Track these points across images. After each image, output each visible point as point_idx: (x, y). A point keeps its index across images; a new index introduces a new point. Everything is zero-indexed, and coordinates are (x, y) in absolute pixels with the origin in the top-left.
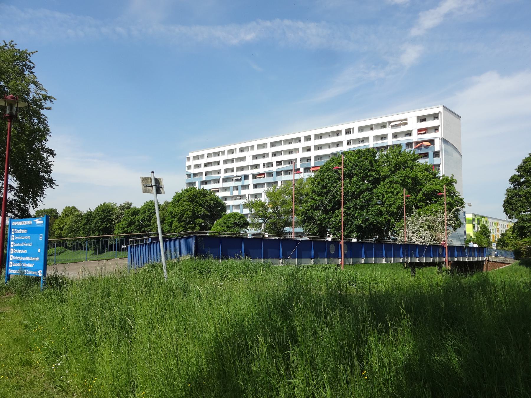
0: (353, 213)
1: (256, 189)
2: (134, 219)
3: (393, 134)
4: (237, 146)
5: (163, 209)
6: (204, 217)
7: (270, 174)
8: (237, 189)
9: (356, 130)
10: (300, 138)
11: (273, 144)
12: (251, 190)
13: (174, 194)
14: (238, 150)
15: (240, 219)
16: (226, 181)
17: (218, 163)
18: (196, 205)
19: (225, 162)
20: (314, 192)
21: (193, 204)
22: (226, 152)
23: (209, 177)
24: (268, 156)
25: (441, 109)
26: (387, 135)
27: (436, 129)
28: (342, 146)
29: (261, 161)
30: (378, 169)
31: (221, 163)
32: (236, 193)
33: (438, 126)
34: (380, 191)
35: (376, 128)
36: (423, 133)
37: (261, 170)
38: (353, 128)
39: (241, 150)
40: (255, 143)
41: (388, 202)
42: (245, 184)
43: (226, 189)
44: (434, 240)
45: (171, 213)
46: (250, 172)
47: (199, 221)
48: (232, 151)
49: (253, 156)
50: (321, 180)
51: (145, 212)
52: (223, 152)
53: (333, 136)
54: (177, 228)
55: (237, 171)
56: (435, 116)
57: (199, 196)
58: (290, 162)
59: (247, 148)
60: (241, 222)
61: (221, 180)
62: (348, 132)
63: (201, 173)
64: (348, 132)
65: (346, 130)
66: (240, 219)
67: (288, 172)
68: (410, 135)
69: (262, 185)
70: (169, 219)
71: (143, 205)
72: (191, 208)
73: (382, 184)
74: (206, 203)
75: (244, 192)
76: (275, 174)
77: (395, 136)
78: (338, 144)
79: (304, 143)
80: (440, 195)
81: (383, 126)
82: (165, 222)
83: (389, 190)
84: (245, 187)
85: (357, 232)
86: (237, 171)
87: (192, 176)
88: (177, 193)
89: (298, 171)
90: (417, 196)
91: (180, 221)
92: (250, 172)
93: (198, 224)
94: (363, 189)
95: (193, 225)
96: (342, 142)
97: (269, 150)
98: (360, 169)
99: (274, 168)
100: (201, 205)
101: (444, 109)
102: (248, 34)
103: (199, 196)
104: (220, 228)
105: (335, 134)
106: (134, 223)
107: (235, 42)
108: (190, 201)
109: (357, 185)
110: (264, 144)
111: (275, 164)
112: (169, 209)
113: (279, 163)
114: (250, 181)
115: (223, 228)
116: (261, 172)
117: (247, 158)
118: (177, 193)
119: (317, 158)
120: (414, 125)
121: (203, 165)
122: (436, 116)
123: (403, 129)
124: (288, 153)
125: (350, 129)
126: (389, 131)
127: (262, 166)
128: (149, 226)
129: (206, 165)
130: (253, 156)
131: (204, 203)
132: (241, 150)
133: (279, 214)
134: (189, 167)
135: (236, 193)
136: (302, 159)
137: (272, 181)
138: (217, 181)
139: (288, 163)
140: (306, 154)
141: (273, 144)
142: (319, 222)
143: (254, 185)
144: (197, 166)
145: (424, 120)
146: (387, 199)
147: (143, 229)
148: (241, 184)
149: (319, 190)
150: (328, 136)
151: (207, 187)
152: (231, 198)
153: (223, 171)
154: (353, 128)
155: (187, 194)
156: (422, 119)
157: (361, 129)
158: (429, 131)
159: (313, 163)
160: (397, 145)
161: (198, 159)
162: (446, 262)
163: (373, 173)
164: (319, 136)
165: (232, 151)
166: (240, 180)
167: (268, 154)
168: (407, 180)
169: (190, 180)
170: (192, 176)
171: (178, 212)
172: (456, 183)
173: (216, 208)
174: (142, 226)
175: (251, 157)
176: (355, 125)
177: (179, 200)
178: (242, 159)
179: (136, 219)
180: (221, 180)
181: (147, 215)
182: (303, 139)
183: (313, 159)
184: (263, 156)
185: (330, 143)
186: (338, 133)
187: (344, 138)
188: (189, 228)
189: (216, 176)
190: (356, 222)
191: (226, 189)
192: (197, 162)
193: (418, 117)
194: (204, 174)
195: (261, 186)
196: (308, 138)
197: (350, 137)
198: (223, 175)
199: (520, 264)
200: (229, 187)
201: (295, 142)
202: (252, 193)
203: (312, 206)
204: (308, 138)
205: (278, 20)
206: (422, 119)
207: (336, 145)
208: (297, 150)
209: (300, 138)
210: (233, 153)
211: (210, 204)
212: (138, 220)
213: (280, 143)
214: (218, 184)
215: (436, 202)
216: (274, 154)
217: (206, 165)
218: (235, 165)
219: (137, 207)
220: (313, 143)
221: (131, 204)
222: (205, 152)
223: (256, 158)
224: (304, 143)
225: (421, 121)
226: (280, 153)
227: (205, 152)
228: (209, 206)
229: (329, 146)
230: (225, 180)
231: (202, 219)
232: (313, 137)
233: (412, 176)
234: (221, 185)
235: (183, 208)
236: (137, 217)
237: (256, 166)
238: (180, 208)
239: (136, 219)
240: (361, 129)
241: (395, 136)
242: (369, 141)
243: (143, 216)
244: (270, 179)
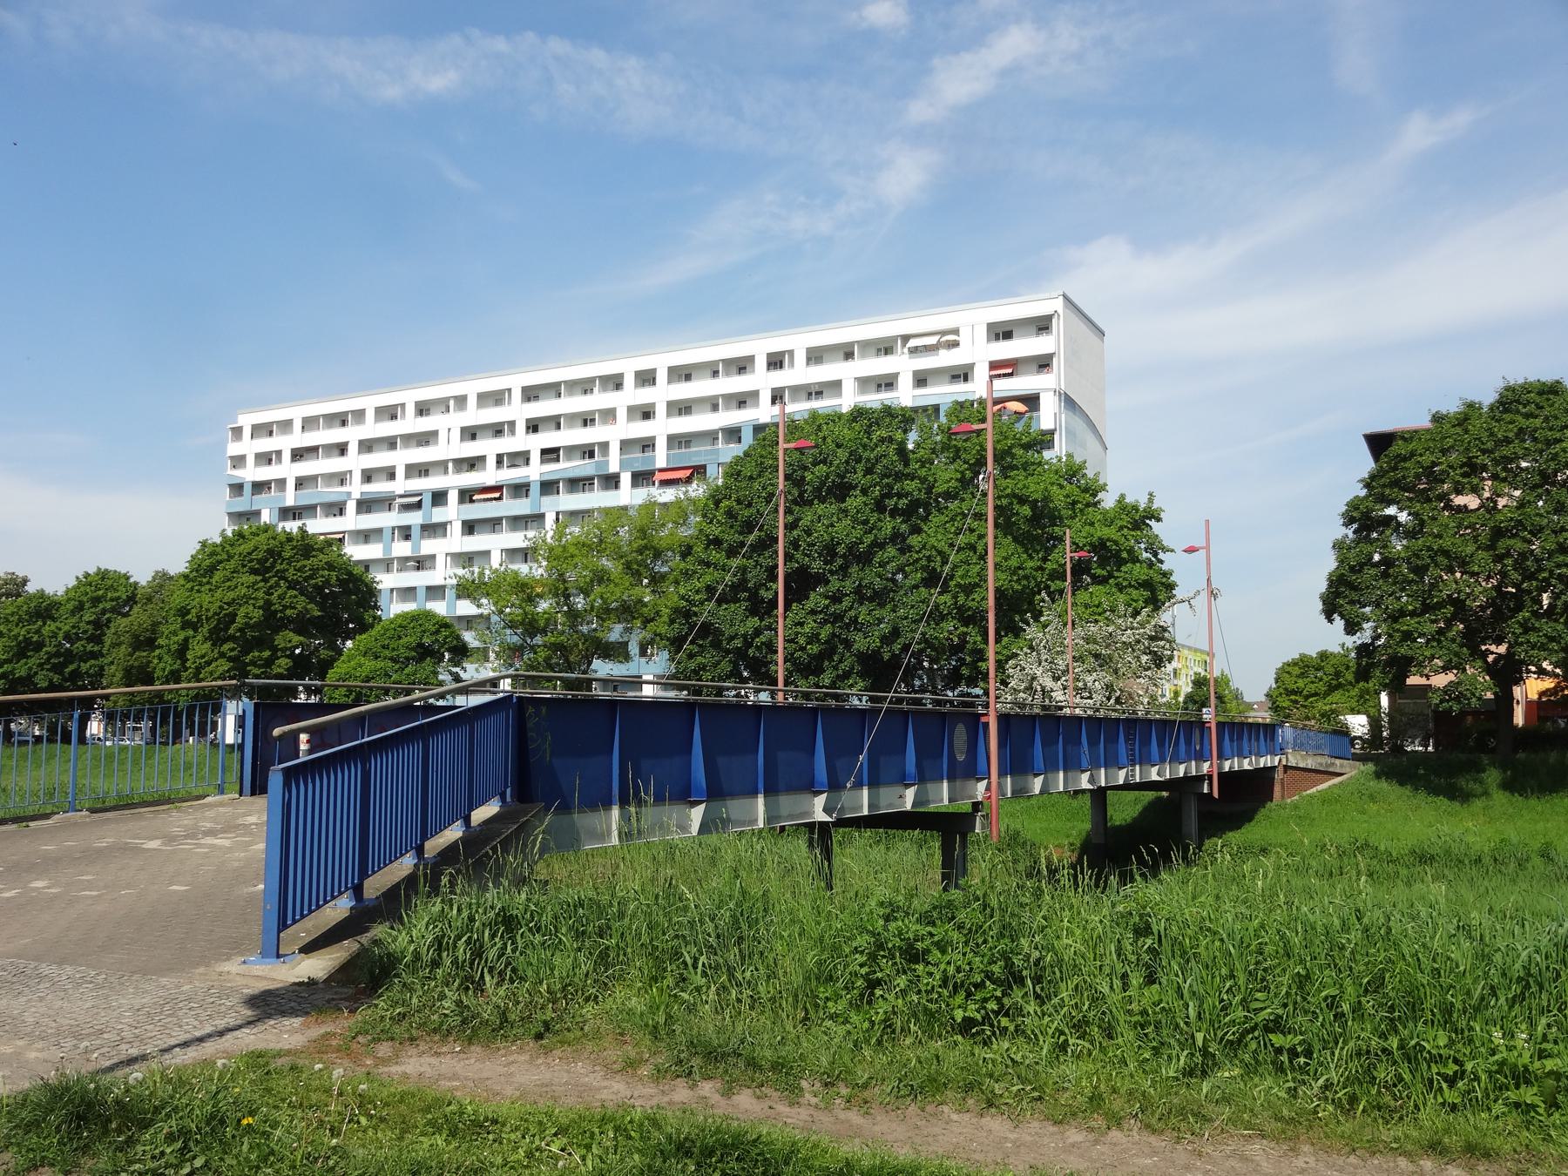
0: (852, 613)
1: (471, 538)
2: (38, 632)
3: (916, 373)
4: (409, 397)
5: (149, 600)
6: (303, 625)
7: (520, 489)
8: (407, 537)
9: (800, 357)
10: (621, 375)
11: (530, 394)
12: (457, 541)
13: (194, 548)
14: (410, 409)
15: (437, 632)
16: (369, 511)
17: (342, 449)
18: (277, 585)
19: (367, 446)
20: (716, 542)
21: (265, 580)
22: (370, 415)
23: (308, 497)
24: (512, 432)
25: (1057, 305)
26: (896, 375)
27: (1043, 363)
28: (756, 404)
29: (488, 447)
30: (923, 472)
31: (353, 448)
32: (402, 549)
33: (1051, 356)
34: (933, 541)
35: (863, 356)
36: (1005, 375)
37: (489, 475)
38: (791, 353)
39: (423, 409)
40: (472, 388)
41: (962, 577)
42: (435, 519)
43: (366, 536)
44: (1118, 701)
45: (183, 612)
46: (454, 481)
47: (288, 638)
48: (390, 413)
49: (463, 430)
50: (739, 502)
51: (80, 607)
52: (359, 415)
53: (727, 374)
54: (209, 663)
55: (407, 477)
56: (1042, 325)
57: (287, 555)
58: (588, 452)
59: (443, 404)
60: (437, 643)
61: (351, 507)
62: (776, 362)
63: (281, 483)
64: (776, 362)
65: (769, 355)
66: (437, 632)
67: (577, 484)
68: (966, 379)
69: (493, 524)
70: (175, 633)
71: (72, 583)
72: (261, 594)
73: (936, 519)
74: (311, 577)
75: (428, 546)
76: (535, 490)
77: (921, 380)
78: (742, 400)
79: (632, 395)
80: (1121, 562)
81: (885, 348)
82: (161, 641)
83: (961, 540)
84: (435, 530)
85: (862, 675)
86: (407, 477)
87: (248, 489)
88: (204, 544)
89: (611, 481)
90: (1045, 560)
91: (217, 637)
92: (454, 481)
93: (284, 650)
94: (881, 536)
95: (267, 654)
96: (755, 394)
97: (518, 411)
98: (869, 471)
99: (535, 471)
100: (292, 585)
101: (1065, 306)
102: (434, 74)
103: (287, 555)
104: (369, 665)
105: (735, 369)
106: (39, 646)
107: (392, 92)
108: (253, 572)
109: (865, 522)
110: (502, 392)
111: (535, 457)
112: (178, 598)
113: (550, 454)
114: (452, 512)
115: (380, 664)
116: (491, 482)
117: (442, 436)
118: (204, 544)
119: (675, 441)
120: (978, 351)
121: (287, 456)
122: (1042, 324)
123: (946, 359)
124: (580, 422)
125: (782, 353)
126: (902, 364)
127: (491, 461)
128: (94, 655)
129: (298, 454)
130: (463, 430)
131: (306, 579)
132: (423, 409)
133: (574, 616)
134: (239, 461)
135: (402, 549)
136: (626, 445)
137: (527, 512)
138: (338, 509)
139: (579, 454)
140: (641, 429)
141: (530, 394)
142: (738, 643)
143: (464, 523)
144: (265, 458)
145: (1008, 335)
146: (955, 567)
147: (72, 667)
148: (420, 521)
149: (731, 537)
150: (709, 372)
151: (318, 526)
152: (387, 564)
153: (357, 476)
154: (791, 353)
155: (245, 548)
156: (1002, 332)
157: (816, 356)
158: (1020, 367)
159: (661, 458)
160: (925, 409)
161: (271, 433)
162: (1210, 777)
163: (911, 486)
164: (682, 374)
165: (390, 413)
166: (418, 505)
167: (512, 424)
168: (1016, 507)
169: (243, 504)
170: (248, 489)
171: (214, 608)
172: (1159, 520)
173: (345, 597)
174: (69, 656)
175: (456, 434)
176: (798, 341)
177: (212, 569)
178: (426, 439)
179: (46, 631)
180: (351, 507)
181: (86, 618)
182: (629, 381)
183: (614, 449)
184: (497, 430)
185: (716, 397)
186: (742, 366)
187: (761, 380)
188: (253, 663)
189: (333, 492)
190: (860, 643)
191: (366, 536)
192: (266, 444)
193: (990, 326)
194: (291, 485)
195: (488, 527)
196: (646, 378)
197: (782, 378)
198: (356, 489)
199: (1378, 775)
200: (379, 531)
201: (604, 389)
202: (458, 550)
203: (710, 590)
204: (646, 378)
205: (530, 36)
206: (1002, 332)
207: (735, 404)
208: (609, 415)
209: (621, 375)
210: (394, 417)
211: (327, 583)
212: (55, 635)
213: (554, 389)
214: (338, 519)
215: (1102, 581)
216: (533, 426)
217: (298, 454)
218: (400, 458)
219: (49, 591)
220: (662, 393)
221: (25, 581)
222: (297, 413)
223: (473, 437)
224: (632, 395)
225: (997, 338)
226: (555, 422)
227: (297, 413)
228: (319, 589)
229: (713, 404)
230: (365, 505)
231: (299, 632)
232: (662, 376)
233: (1035, 496)
234: (351, 520)
235: (231, 595)
236: (51, 626)
237: (473, 463)
238: (218, 594)
239: (46, 631)
240: (816, 356)
241: (921, 380)
242: (840, 395)
243: (74, 620)
244: (521, 507)
